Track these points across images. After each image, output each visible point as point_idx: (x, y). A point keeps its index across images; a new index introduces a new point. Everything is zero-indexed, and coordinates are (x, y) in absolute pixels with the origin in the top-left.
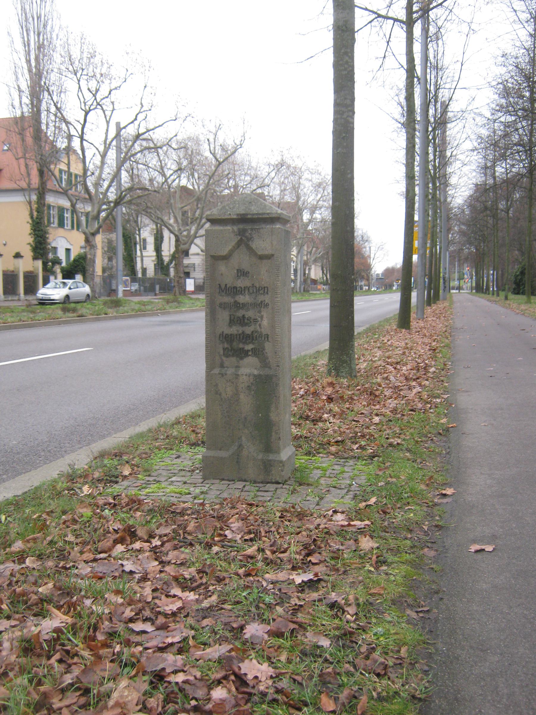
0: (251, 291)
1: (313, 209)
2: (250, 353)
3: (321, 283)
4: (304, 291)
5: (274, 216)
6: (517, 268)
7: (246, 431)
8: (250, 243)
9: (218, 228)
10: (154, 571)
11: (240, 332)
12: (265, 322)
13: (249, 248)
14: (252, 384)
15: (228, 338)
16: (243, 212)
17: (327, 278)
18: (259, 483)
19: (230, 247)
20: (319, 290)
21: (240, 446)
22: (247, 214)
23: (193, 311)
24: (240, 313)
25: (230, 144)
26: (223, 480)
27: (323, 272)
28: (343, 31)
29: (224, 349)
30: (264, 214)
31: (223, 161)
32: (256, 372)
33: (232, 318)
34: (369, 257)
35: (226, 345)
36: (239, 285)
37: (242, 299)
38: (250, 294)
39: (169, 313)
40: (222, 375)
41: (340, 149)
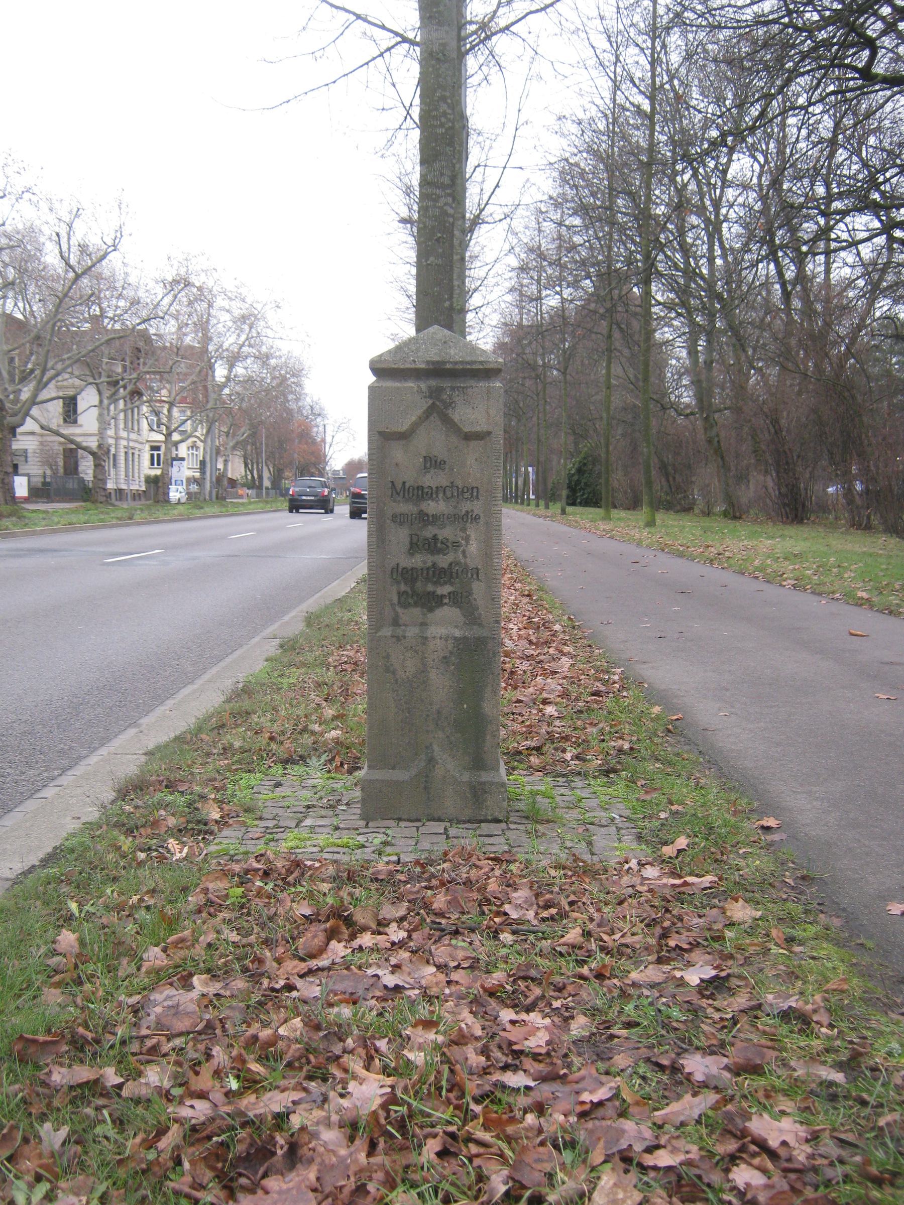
0: (449, 494)
1: (233, 360)
2: (446, 601)
3: (244, 485)
4: (217, 498)
5: (491, 366)
6: (571, 466)
7: (440, 734)
8: (450, 411)
9: (389, 384)
10: (437, 983)
11: (429, 564)
12: (473, 548)
13: (447, 420)
14: (451, 653)
15: (407, 575)
16: (437, 359)
17: (253, 477)
18: (464, 822)
19: (414, 419)
20: (241, 497)
21: (431, 761)
22: (444, 363)
23: (54, 531)
24: (429, 531)
25: (94, 241)
26: (400, 819)
27: (246, 465)
28: (438, 59)
29: (400, 594)
30: (475, 362)
31: (84, 273)
32: (457, 633)
33: (415, 540)
34: (324, 441)
35: (403, 587)
36: (427, 484)
37: (432, 507)
38: (447, 499)
39: (13, 535)
40: (398, 639)
41: (432, 259)
